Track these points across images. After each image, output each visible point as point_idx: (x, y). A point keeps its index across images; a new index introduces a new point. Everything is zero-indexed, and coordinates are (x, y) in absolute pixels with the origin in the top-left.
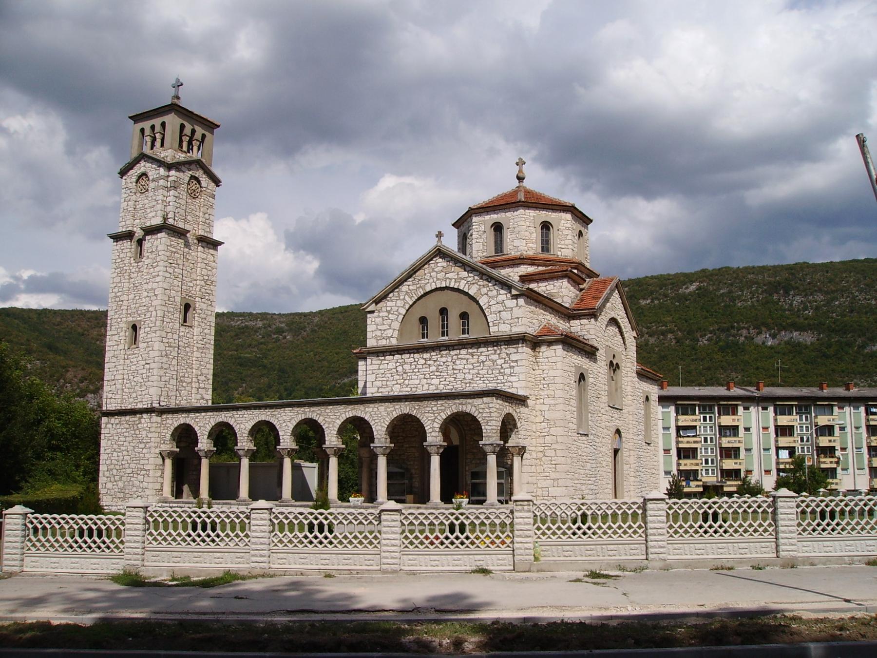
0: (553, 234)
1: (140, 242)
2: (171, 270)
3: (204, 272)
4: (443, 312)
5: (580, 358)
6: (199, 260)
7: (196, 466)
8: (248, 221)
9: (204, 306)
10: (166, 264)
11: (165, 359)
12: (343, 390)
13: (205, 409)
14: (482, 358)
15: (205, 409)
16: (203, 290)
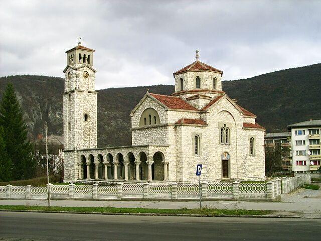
1: (70, 95)
4: (150, 116)
7: (90, 167)
12: (128, 143)
13: (96, 150)
14: (159, 132)
15: (96, 150)
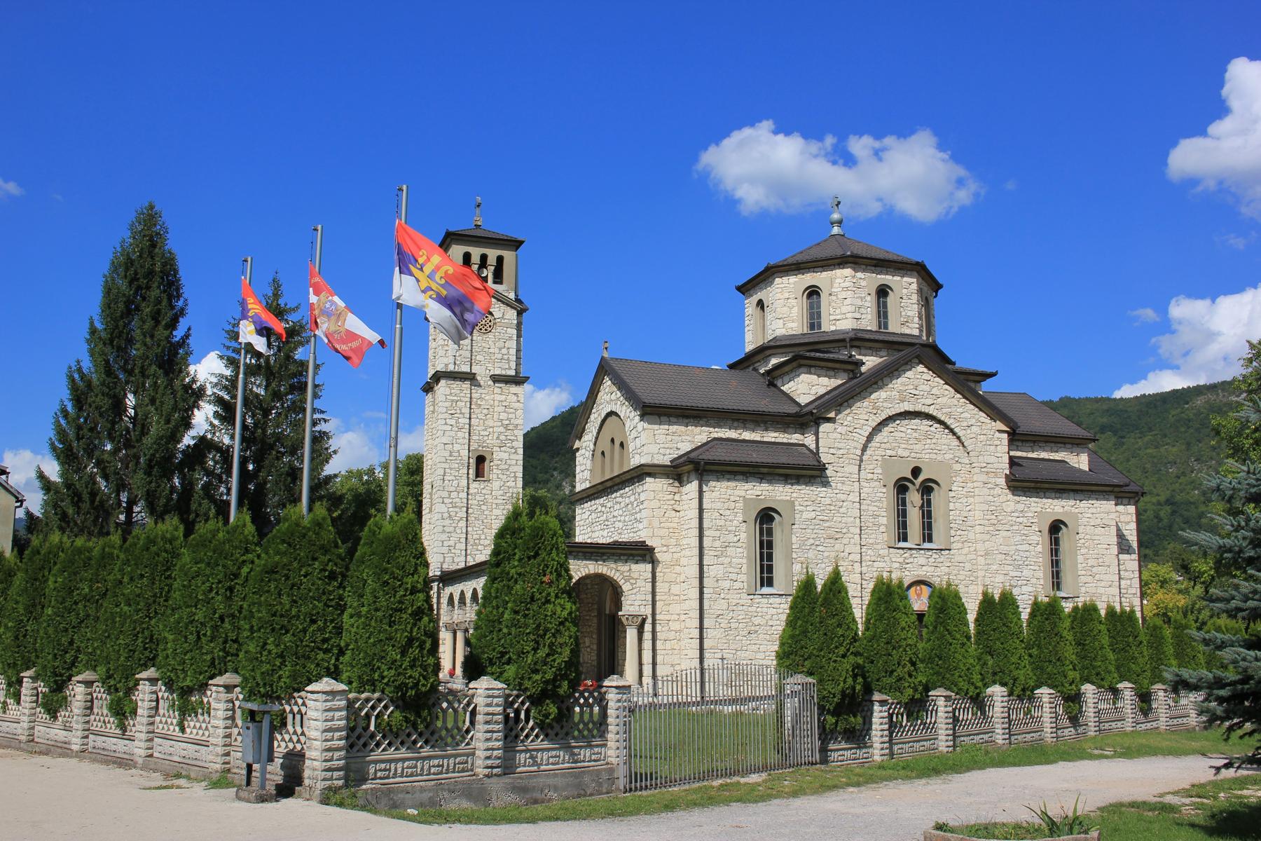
0: (891, 299)
2: (453, 422)
3: (503, 416)
5: (748, 486)
6: (496, 403)
8: (1213, 301)
9: (505, 456)
10: (447, 416)
11: (447, 522)
16: (502, 437)
